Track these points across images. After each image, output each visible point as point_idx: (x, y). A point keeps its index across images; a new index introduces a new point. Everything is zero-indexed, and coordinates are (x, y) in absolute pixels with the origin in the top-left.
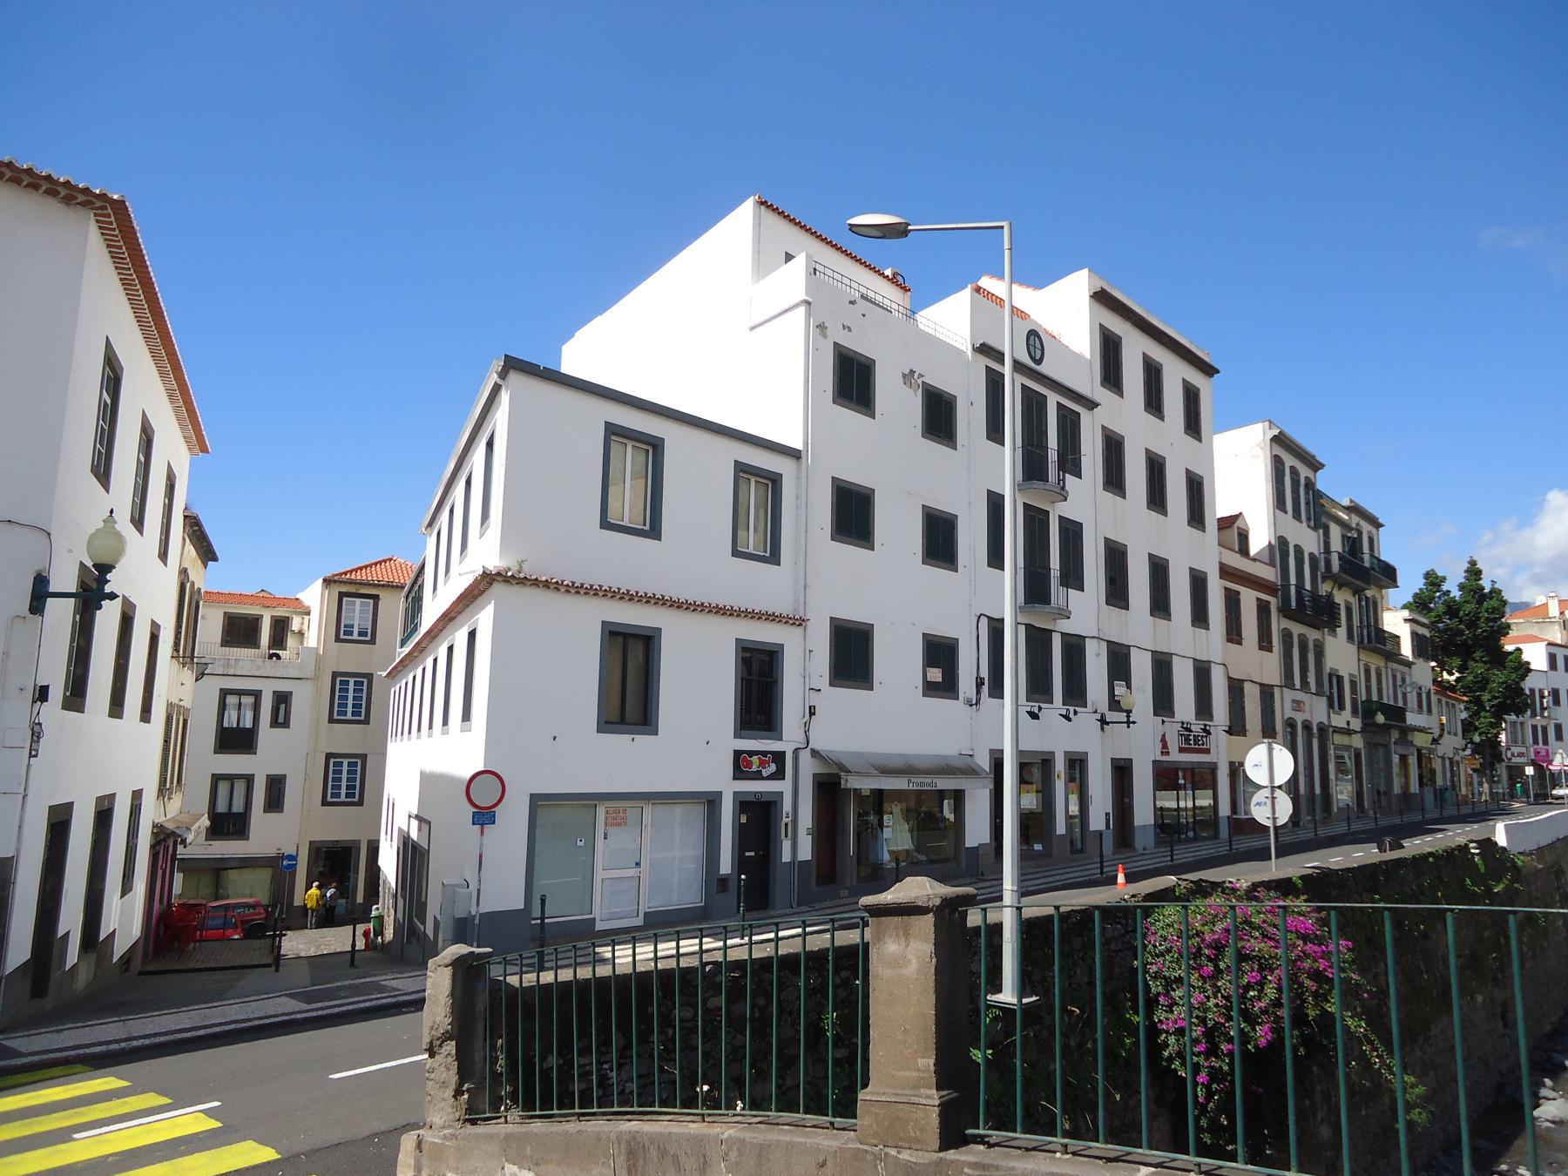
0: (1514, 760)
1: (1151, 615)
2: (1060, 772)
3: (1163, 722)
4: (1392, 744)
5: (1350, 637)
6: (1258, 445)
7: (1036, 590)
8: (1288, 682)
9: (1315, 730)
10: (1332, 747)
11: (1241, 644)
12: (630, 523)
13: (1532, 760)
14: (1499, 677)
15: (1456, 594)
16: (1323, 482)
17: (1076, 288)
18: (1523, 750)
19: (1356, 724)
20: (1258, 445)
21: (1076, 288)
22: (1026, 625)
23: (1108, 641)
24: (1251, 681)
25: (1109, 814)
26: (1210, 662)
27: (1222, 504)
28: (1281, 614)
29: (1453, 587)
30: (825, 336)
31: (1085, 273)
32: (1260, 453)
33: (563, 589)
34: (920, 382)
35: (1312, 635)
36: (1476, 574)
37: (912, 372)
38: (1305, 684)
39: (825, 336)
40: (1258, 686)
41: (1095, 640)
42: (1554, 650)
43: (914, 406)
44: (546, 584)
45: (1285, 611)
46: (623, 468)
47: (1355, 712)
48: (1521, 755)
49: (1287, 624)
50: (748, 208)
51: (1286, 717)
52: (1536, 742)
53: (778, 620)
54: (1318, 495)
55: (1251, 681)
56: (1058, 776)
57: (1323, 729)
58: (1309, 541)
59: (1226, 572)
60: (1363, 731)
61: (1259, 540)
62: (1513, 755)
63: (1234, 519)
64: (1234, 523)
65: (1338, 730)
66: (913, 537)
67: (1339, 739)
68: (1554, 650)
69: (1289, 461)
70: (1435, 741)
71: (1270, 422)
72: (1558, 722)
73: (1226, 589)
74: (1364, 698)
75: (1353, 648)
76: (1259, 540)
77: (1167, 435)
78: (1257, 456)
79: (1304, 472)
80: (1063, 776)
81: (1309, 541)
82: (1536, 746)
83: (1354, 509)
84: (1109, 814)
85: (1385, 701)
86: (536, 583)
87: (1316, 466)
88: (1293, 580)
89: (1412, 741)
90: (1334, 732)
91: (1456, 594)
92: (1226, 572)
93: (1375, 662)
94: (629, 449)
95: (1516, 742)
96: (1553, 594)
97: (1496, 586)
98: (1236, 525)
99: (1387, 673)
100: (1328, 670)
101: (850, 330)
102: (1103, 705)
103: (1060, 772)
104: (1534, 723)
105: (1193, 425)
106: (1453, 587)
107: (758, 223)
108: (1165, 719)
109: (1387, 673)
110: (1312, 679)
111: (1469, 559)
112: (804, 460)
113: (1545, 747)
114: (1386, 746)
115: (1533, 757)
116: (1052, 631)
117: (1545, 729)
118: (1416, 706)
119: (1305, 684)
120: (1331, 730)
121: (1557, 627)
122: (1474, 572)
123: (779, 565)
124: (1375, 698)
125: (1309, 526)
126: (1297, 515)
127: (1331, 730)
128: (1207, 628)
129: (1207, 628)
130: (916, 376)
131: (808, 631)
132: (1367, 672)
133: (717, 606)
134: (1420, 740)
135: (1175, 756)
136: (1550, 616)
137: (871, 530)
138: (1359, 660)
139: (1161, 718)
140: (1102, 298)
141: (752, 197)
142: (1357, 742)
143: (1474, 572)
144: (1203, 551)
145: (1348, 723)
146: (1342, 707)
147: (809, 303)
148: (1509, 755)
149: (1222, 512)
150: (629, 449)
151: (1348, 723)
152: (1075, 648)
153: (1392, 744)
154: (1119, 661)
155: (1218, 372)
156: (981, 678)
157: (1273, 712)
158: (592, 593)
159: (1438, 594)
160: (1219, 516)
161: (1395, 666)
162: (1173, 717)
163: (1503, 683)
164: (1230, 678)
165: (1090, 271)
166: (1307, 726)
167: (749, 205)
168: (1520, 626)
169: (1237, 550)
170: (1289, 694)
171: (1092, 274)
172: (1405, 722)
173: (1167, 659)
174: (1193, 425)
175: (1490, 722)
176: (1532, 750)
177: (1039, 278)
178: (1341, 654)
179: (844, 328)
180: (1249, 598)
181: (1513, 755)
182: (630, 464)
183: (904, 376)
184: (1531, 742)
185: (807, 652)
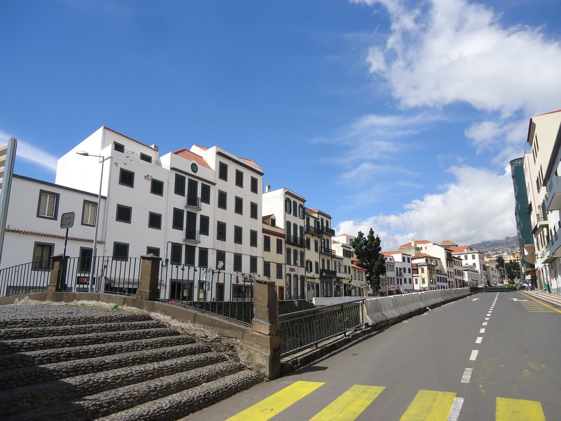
0: (391, 289)
1: (234, 243)
2: (196, 286)
3: (237, 273)
4: (333, 282)
5: (316, 250)
6: (282, 195)
7: (190, 234)
8: (288, 262)
9: (299, 277)
10: (306, 282)
11: (270, 252)
12: (47, 215)
13: (397, 289)
14: (377, 263)
15: (367, 239)
16: (306, 205)
17: (213, 150)
18: (394, 286)
19: (317, 276)
20: (282, 195)
21: (213, 150)
22: (186, 245)
23: (217, 250)
24: (273, 262)
25: (214, 298)
26: (257, 257)
27: (264, 211)
28: (286, 243)
29: (366, 236)
30: (117, 166)
31: (215, 147)
32: (282, 196)
33: (52, 236)
34: (151, 178)
35: (299, 250)
36: (372, 233)
37: (148, 176)
38: (295, 264)
39: (117, 166)
40: (276, 264)
41: (212, 250)
42: (404, 256)
43: (149, 185)
44: (36, 234)
45: (288, 242)
46: (46, 201)
47: (317, 272)
48: (393, 288)
49: (288, 246)
50: (101, 130)
51: (287, 273)
52: (398, 284)
53: (99, 243)
54: (304, 209)
55: (273, 262)
56: (195, 287)
57: (303, 278)
58: (300, 222)
59: (264, 231)
60: (320, 278)
61: (280, 223)
62: (390, 288)
63: (268, 217)
64: (270, 217)
65: (308, 277)
66: (146, 220)
67: (309, 280)
68: (404, 256)
69: (292, 199)
70: (350, 282)
71: (285, 188)
72: (405, 278)
73: (264, 236)
74: (321, 268)
75: (317, 254)
76: (280, 223)
77: (245, 193)
78: (282, 198)
79: (299, 202)
80: (197, 287)
81: (300, 222)
82: (398, 285)
83: (319, 213)
84: (214, 298)
85: (331, 270)
86: (13, 231)
87: (304, 201)
88: (292, 234)
89: (342, 282)
90: (307, 278)
91: (367, 239)
92: (264, 231)
93: (326, 258)
94: (48, 197)
95: (392, 284)
96: (413, 239)
97: (378, 236)
98: (270, 218)
99: (332, 261)
100: (306, 260)
101: (126, 164)
102: (214, 268)
103: (196, 286)
104: (398, 278)
105: (254, 188)
106: (366, 236)
107: (104, 134)
108: (238, 272)
109: (332, 261)
110: (299, 262)
111: (370, 228)
112: (107, 199)
113: (401, 285)
114: (331, 283)
115: (397, 288)
116: (195, 247)
117: (401, 280)
118: (344, 272)
119: (295, 264)
120: (306, 277)
121: (414, 249)
122: (372, 232)
123: (208, 235)
124: (326, 268)
125: (300, 218)
126: (295, 214)
127: (306, 277)
128: (256, 246)
129: (256, 246)
130: (149, 177)
131: (105, 245)
132: (323, 261)
133: (83, 239)
134: (345, 282)
135: (241, 282)
136: (412, 246)
137: (130, 218)
138: (320, 257)
139: (237, 272)
140: (219, 153)
141: (103, 127)
142: (317, 281)
143: (372, 232)
144: (258, 225)
145: (314, 276)
146: (311, 271)
147: (112, 158)
148: (389, 288)
149: (265, 214)
150: (48, 197)
151: (314, 276)
152: (204, 253)
153: (333, 282)
154: (221, 256)
155: (264, 174)
156: (167, 259)
157: (282, 272)
158: (34, 234)
159: (362, 239)
160: (263, 216)
161: (335, 259)
162: (257, 273)
163: (377, 265)
164: (264, 261)
165: (217, 146)
166: (296, 276)
167: (102, 128)
168: (404, 249)
169: (271, 225)
170: (288, 267)
171: (217, 147)
172: (336, 276)
173: (255, 258)
174: (254, 188)
175: (375, 277)
176: (397, 286)
177: (206, 147)
178: (312, 255)
179: (124, 164)
180: (273, 240)
181: (390, 288)
182: (48, 200)
183: (145, 176)
184: (396, 284)
185: (105, 251)
